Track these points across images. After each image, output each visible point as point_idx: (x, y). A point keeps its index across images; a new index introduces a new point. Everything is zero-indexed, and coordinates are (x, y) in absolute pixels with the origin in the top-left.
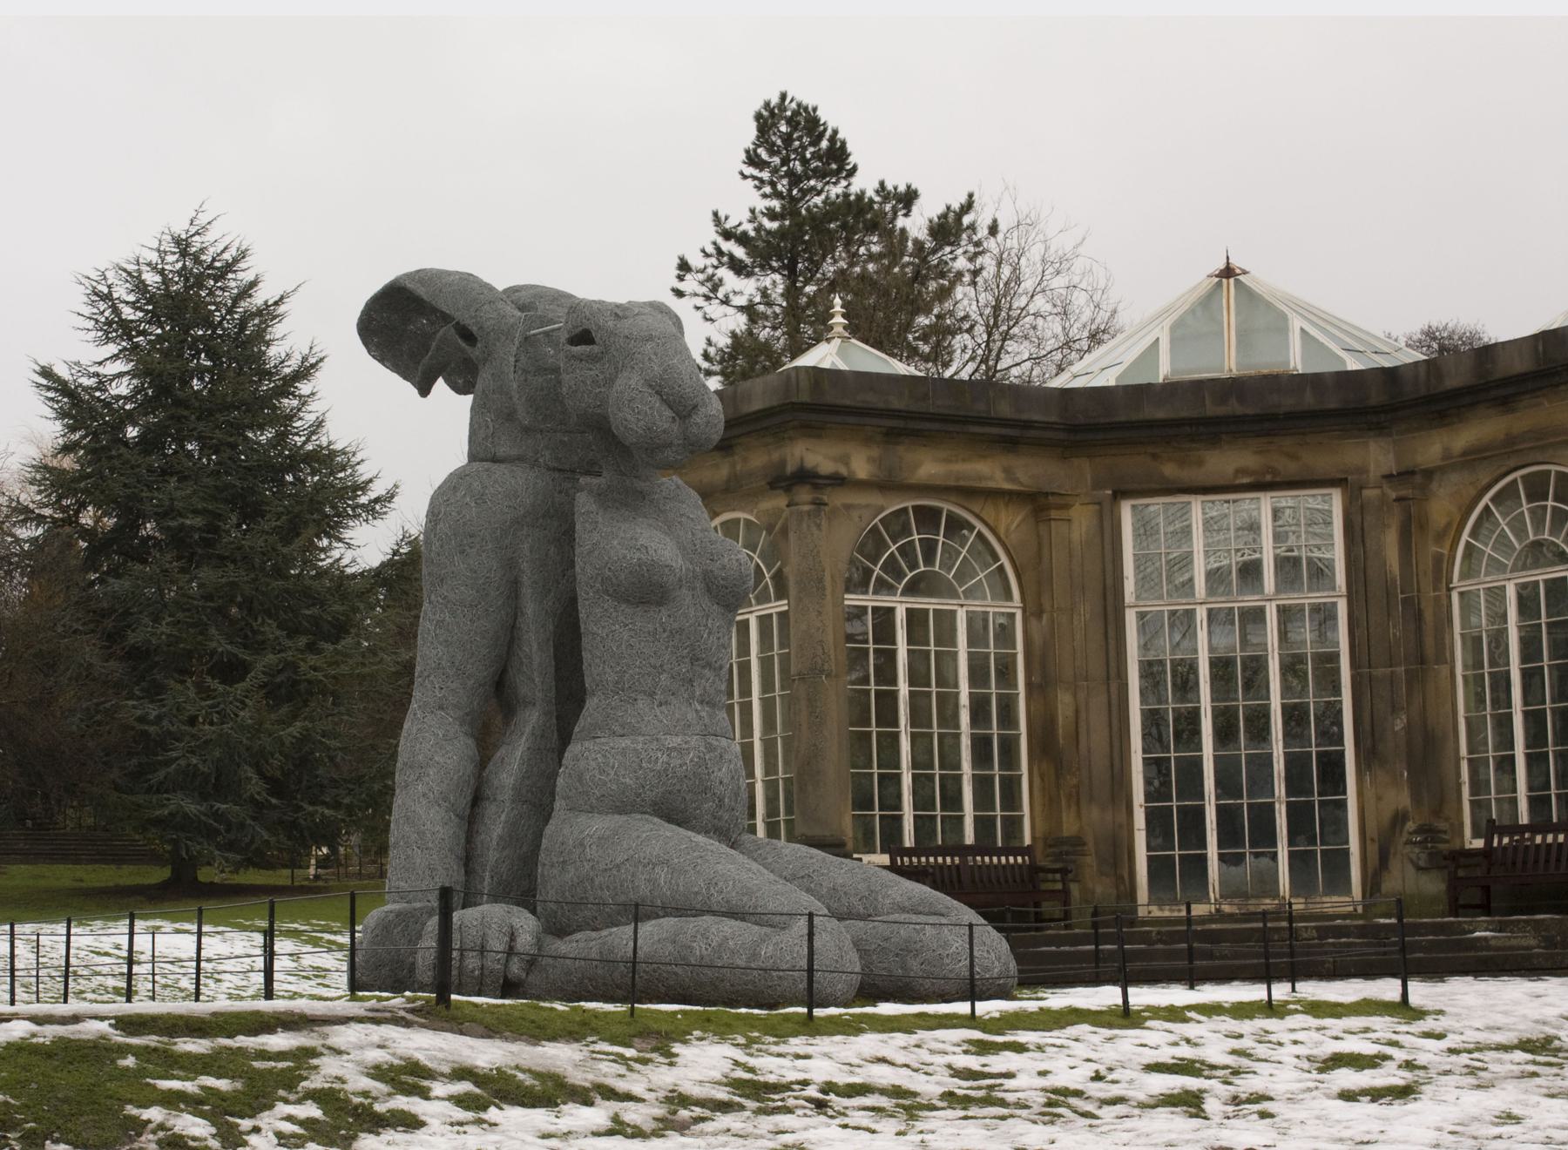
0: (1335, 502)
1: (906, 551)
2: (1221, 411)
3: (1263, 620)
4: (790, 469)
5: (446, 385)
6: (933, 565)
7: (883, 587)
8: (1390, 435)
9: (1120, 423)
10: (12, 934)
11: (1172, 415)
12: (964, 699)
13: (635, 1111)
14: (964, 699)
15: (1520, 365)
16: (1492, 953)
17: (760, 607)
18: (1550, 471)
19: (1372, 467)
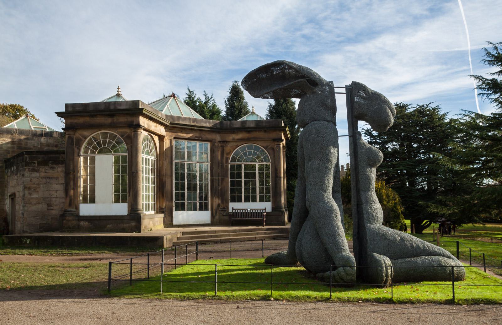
0: (209, 144)
1: (110, 142)
2: (193, 124)
3: (259, 169)
4: (135, 123)
5: (299, 101)
6: (101, 146)
7: (239, 161)
8: (220, 134)
9: (175, 123)
10: (453, 285)
11: (185, 123)
12: (186, 180)
13: (86, 262)
14: (186, 180)
15: (252, 125)
16: (490, 236)
17: (179, 162)
18: (108, 133)
19: (217, 139)
